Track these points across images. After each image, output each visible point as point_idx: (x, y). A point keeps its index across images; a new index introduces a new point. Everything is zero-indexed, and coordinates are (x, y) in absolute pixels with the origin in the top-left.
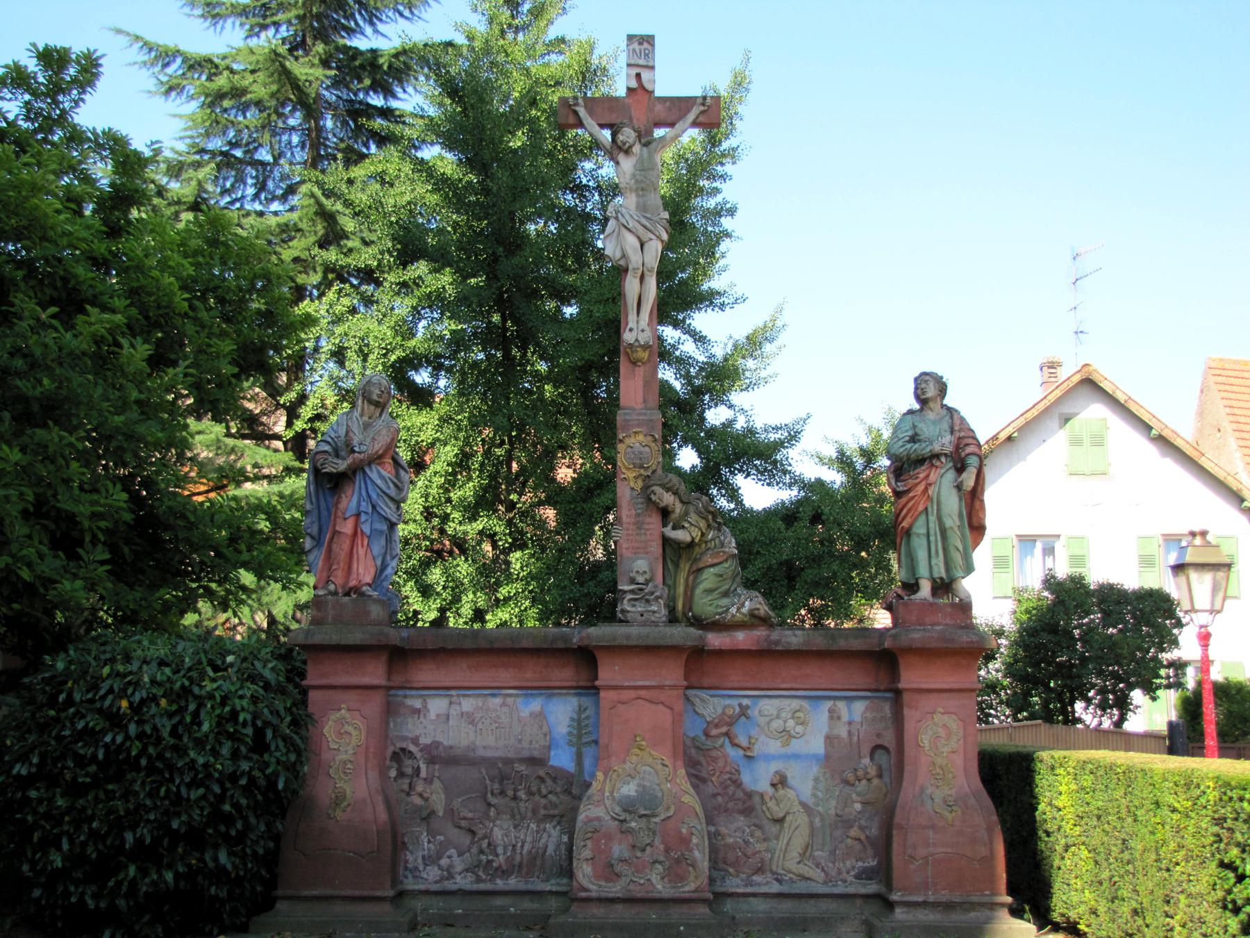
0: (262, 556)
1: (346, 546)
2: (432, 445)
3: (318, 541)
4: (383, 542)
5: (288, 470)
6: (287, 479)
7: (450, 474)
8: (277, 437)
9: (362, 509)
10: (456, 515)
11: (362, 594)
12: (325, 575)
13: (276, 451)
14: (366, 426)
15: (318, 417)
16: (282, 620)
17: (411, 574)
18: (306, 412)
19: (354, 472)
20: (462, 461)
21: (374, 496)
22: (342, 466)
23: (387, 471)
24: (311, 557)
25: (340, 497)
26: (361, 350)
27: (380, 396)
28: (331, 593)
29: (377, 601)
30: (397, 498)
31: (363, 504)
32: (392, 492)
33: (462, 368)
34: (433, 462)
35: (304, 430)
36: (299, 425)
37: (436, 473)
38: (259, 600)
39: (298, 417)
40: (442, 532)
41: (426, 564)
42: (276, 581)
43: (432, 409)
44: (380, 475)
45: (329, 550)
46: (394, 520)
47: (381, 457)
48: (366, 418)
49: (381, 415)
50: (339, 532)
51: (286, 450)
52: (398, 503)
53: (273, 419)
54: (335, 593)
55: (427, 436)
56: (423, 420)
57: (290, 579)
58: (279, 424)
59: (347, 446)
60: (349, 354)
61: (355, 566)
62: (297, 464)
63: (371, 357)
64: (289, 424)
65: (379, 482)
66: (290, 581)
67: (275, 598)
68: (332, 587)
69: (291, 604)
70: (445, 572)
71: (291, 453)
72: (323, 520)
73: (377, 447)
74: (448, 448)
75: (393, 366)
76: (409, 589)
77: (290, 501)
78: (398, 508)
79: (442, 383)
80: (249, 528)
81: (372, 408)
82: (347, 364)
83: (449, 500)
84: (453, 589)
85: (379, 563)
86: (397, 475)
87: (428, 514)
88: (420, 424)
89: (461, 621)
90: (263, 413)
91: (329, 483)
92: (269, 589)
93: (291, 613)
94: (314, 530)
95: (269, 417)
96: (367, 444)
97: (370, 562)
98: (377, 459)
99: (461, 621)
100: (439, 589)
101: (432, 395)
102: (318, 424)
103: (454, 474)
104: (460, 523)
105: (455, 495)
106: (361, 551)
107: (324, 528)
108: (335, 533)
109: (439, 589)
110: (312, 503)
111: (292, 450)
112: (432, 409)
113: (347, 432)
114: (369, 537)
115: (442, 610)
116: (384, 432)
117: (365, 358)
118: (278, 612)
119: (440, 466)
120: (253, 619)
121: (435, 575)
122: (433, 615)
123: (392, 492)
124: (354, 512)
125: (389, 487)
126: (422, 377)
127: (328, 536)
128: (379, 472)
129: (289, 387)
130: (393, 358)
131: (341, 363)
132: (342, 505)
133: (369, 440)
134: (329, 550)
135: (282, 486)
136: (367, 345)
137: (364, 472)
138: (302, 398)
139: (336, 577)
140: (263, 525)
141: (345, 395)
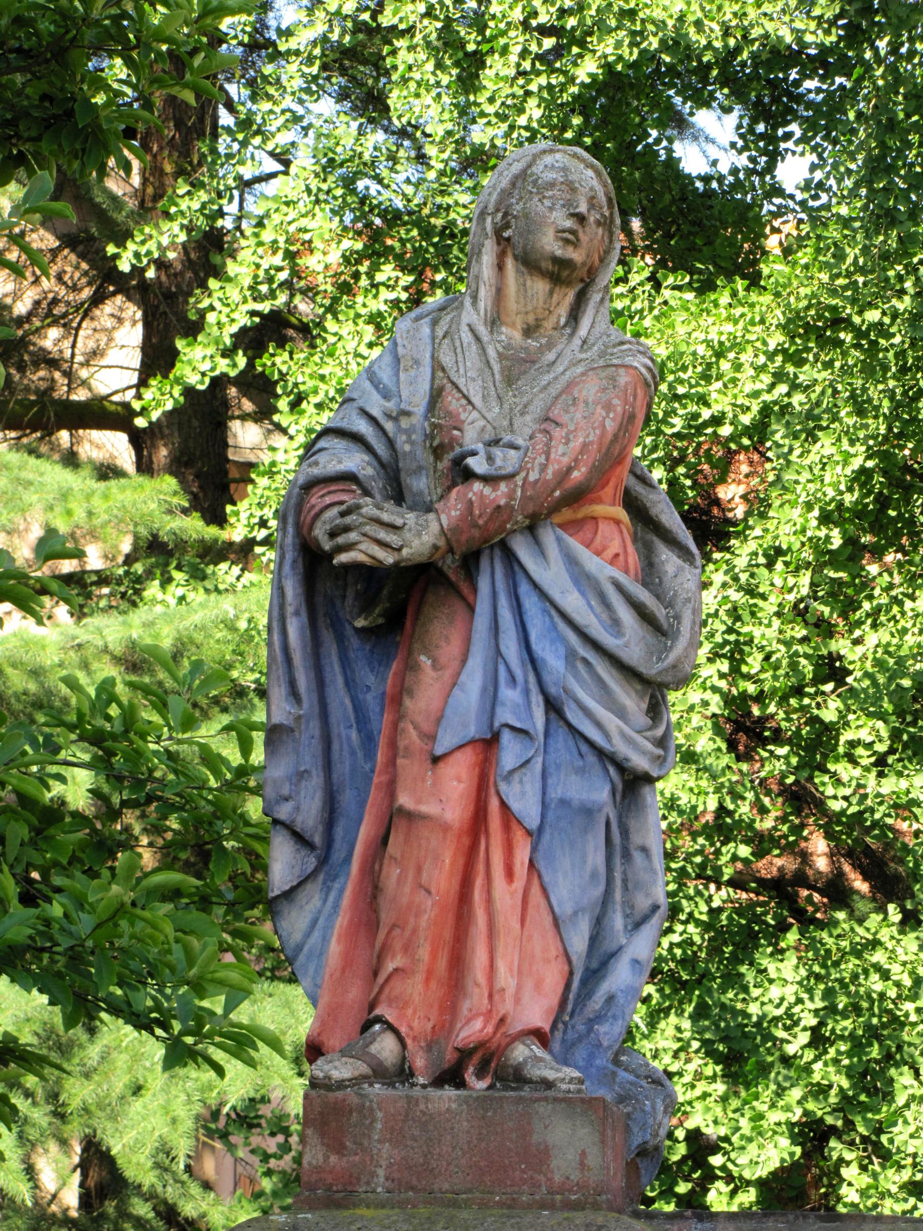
0: (85, 923)
1: (441, 874)
2: (759, 431)
3: (321, 850)
4: (596, 857)
5: (157, 552)
6: (153, 589)
7: (835, 559)
8: (116, 417)
9: (505, 716)
10: (867, 731)
11: (515, 1078)
12: (355, 994)
13: (107, 472)
14: (515, 368)
15: (269, 331)
16: (148, 1179)
17: (681, 981)
18: (228, 306)
19: (470, 562)
20: (883, 502)
21: (553, 661)
22: (419, 536)
23: (607, 551)
24: (296, 921)
25: (411, 666)
26: (449, 40)
27: (570, 239)
28: (379, 1073)
29: (580, 1105)
30: (651, 670)
31: (509, 694)
32: (632, 642)
33: (883, 96)
34: (758, 505)
35: (219, 383)
36: (198, 362)
37: (774, 554)
38: (53, 1096)
39: (193, 329)
40: (801, 799)
41: (738, 942)
42: (142, 1023)
43: (754, 281)
44: (576, 573)
45: (372, 889)
46: (640, 763)
47: (578, 496)
48: (512, 334)
49: (575, 316)
50: (410, 816)
51: (145, 467)
52: (654, 692)
53: (86, 340)
54: (402, 1073)
55: (735, 397)
56: (718, 328)
57: (202, 1016)
58: (110, 355)
59: (438, 452)
60: (403, 56)
61: (479, 957)
62: (194, 526)
63: (497, 71)
64: (157, 359)
65: (573, 601)
66: (198, 1021)
67: (120, 1083)
68: (385, 1047)
69: (187, 1115)
70: (821, 971)
71: (170, 483)
72: (343, 768)
73: (561, 454)
74: (825, 445)
75: (582, 104)
76: (668, 1041)
77: (170, 680)
78: (656, 709)
79: (793, 171)
80: (25, 800)
81: (540, 286)
82: (395, 99)
83: (832, 670)
84: (858, 1046)
85: (579, 943)
86: (650, 573)
87: (744, 730)
88: (711, 343)
89: (892, 1179)
90: (48, 312)
91: (366, 606)
92: (93, 1052)
93: (183, 1147)
94: (308, 811)
95: (73, 331)
96: (528, 434)
97: (543, 942)
98: (564, 504)
99: (892, 1179)
100: (797, 1044)
101: (750, 223)
102: (277, 361)
103: (853, 553)
104: (881, 762)
105: (858, 650)
106: (506, 896)
107: (347, 798)
108: (394, 818)
109: (797, 1044)
110: (294, 693)
111: (176, 467)
112: (754, 281)
113: (436, 395)
114: (535, 836)
115: (812, 1135)
116: (590, 389)
117: (470, 68)
118: (133, 1144)
119: (790, 524)
120: (30, 1171)
121: (779, 984)
122: (773, 1154)
123: (632, 642)
124: (473, 731)
125: (615, 624)
126: (709, 144)
127: (365, 832)
128: (572, 561)
129: (152, 204)
130: (587, 69)
131: (371, 105)
132: (423, 700)
133: (526, 425)
134: (372, 889)
135: (138, 616)
136: (479, 22)
137: (510, 558)
138: (209, 250)
139: (402, 1004)
140: (77, 788)
141: (378, 233)
